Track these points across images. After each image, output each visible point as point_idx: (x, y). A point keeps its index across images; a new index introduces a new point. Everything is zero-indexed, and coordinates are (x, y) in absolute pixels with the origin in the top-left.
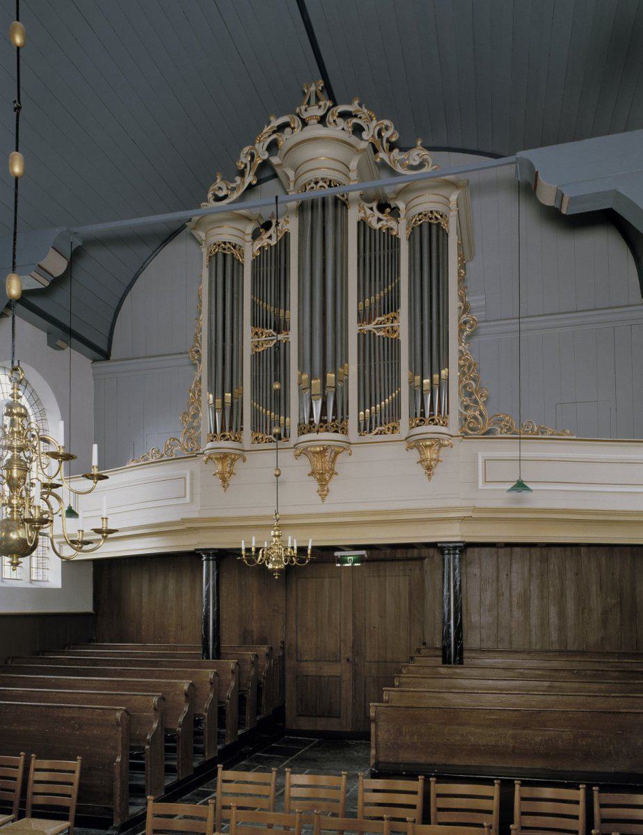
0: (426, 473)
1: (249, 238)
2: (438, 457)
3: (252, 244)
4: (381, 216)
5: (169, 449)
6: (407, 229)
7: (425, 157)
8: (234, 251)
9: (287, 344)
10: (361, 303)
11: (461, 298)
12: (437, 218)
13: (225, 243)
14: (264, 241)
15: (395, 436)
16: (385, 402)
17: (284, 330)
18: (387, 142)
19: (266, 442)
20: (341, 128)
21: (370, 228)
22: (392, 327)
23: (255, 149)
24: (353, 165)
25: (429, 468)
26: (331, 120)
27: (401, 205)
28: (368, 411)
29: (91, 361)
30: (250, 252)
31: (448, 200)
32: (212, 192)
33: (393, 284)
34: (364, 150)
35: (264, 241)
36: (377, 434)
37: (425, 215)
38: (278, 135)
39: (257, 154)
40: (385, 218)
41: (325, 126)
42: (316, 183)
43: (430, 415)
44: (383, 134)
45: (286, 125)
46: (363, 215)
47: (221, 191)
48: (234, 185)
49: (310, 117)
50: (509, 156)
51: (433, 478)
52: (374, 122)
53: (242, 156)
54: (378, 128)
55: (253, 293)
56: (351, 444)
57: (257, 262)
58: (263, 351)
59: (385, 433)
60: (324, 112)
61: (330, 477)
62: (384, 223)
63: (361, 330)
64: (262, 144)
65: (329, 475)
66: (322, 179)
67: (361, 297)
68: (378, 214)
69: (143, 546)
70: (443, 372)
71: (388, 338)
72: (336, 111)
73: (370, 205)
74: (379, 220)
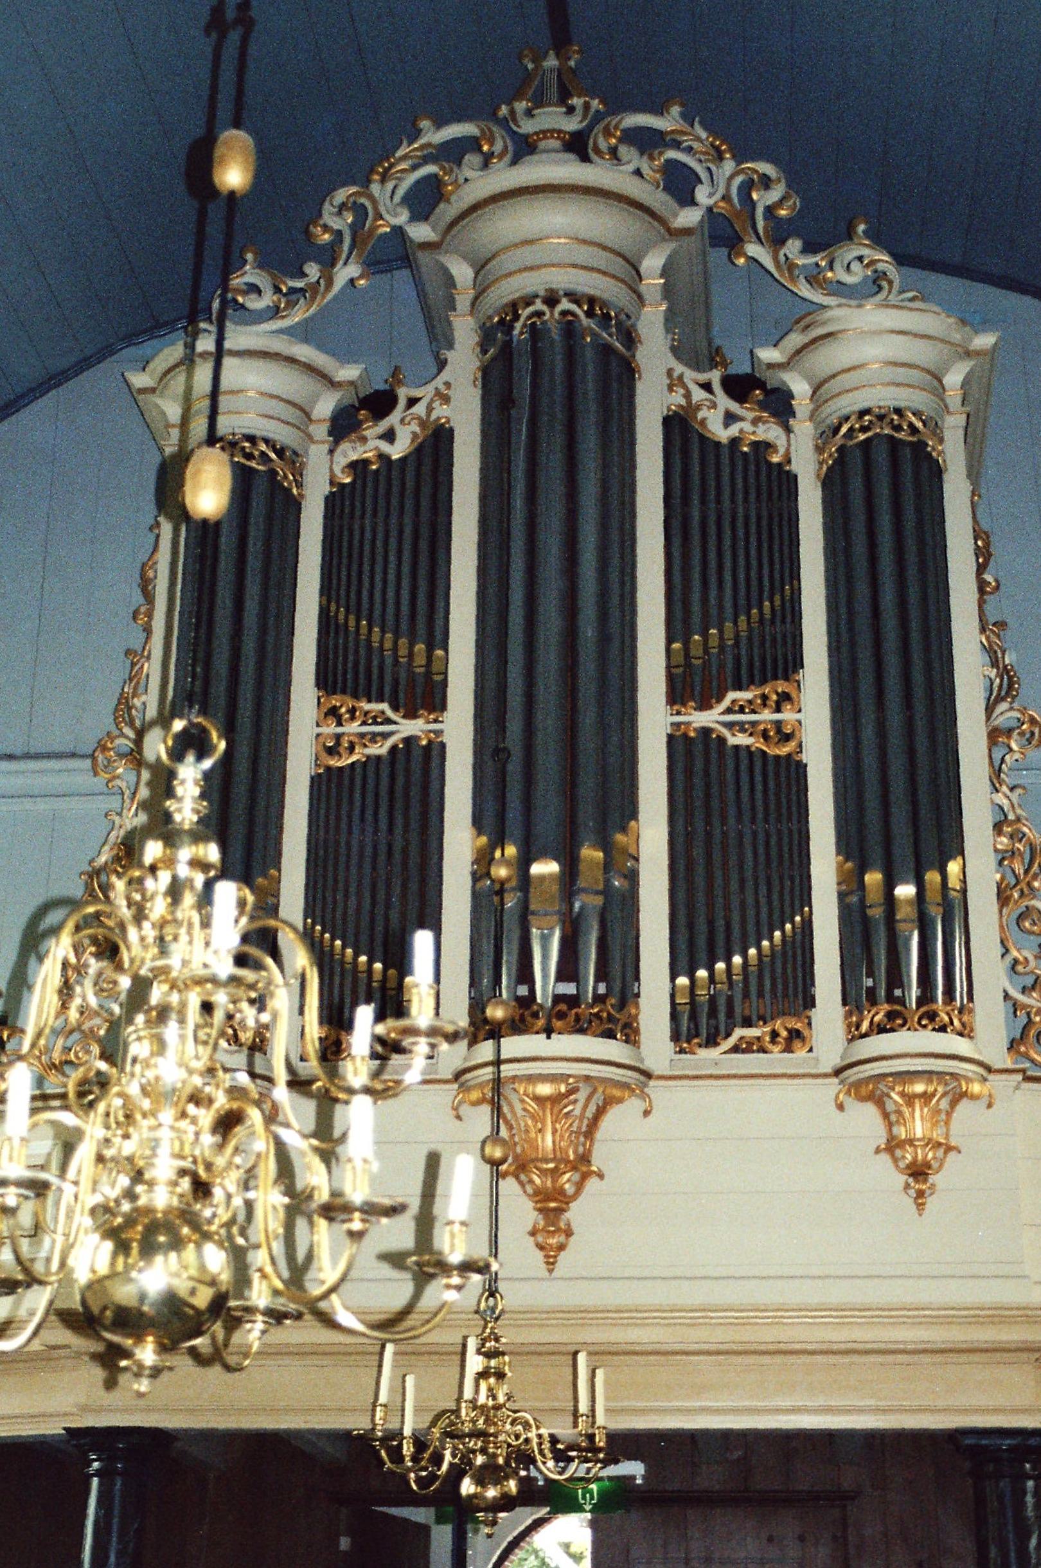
0: (907, 1186)
1: (320, 431)
2: (947, 1136)
3: (331, 452)
4: (734, 407)
6: (819, 449)
7: (881, 266)
11: (993, 656)
12: (913, 430)
13: (252, 439)
18: (765, 218)
20: (631, 168)
21: (703, 438)
22: (778, 724)
23: (371, 197)
24: (653, 263)
25: (919, 1172)
26: (603, 145)
27: (800, 388)
31: (940, 381)
33: (777, 598)
34: (687, 232)
36: (735, 1049)
37: (881, 418)
38: (442, 168)
39: (376, 209)
40: (750, 415)
41: (585, 158)
43: (921, 1002)
44: (755, 196)
45: (471, 144)
46: (683, 402)
47: (253, 296)
48: (299, 284)
49: (544, 132)
50: (156, 354)
51: (931, 1202)
52: (729, 166)
53: (327, 208)
54: (739, 179)
56: (648, 1075)
57: (335, 502)
59: (763, 1050)
61: (579, 1186)
62: (747, 426)
64: (390, 185)
65: (577, 1177)
66: (566, 295)
68: (725, 402)
69: (1001, 1401)
70: (953, 867)
72: (616, 127)
73: (703, 377)
74: (730, 418)
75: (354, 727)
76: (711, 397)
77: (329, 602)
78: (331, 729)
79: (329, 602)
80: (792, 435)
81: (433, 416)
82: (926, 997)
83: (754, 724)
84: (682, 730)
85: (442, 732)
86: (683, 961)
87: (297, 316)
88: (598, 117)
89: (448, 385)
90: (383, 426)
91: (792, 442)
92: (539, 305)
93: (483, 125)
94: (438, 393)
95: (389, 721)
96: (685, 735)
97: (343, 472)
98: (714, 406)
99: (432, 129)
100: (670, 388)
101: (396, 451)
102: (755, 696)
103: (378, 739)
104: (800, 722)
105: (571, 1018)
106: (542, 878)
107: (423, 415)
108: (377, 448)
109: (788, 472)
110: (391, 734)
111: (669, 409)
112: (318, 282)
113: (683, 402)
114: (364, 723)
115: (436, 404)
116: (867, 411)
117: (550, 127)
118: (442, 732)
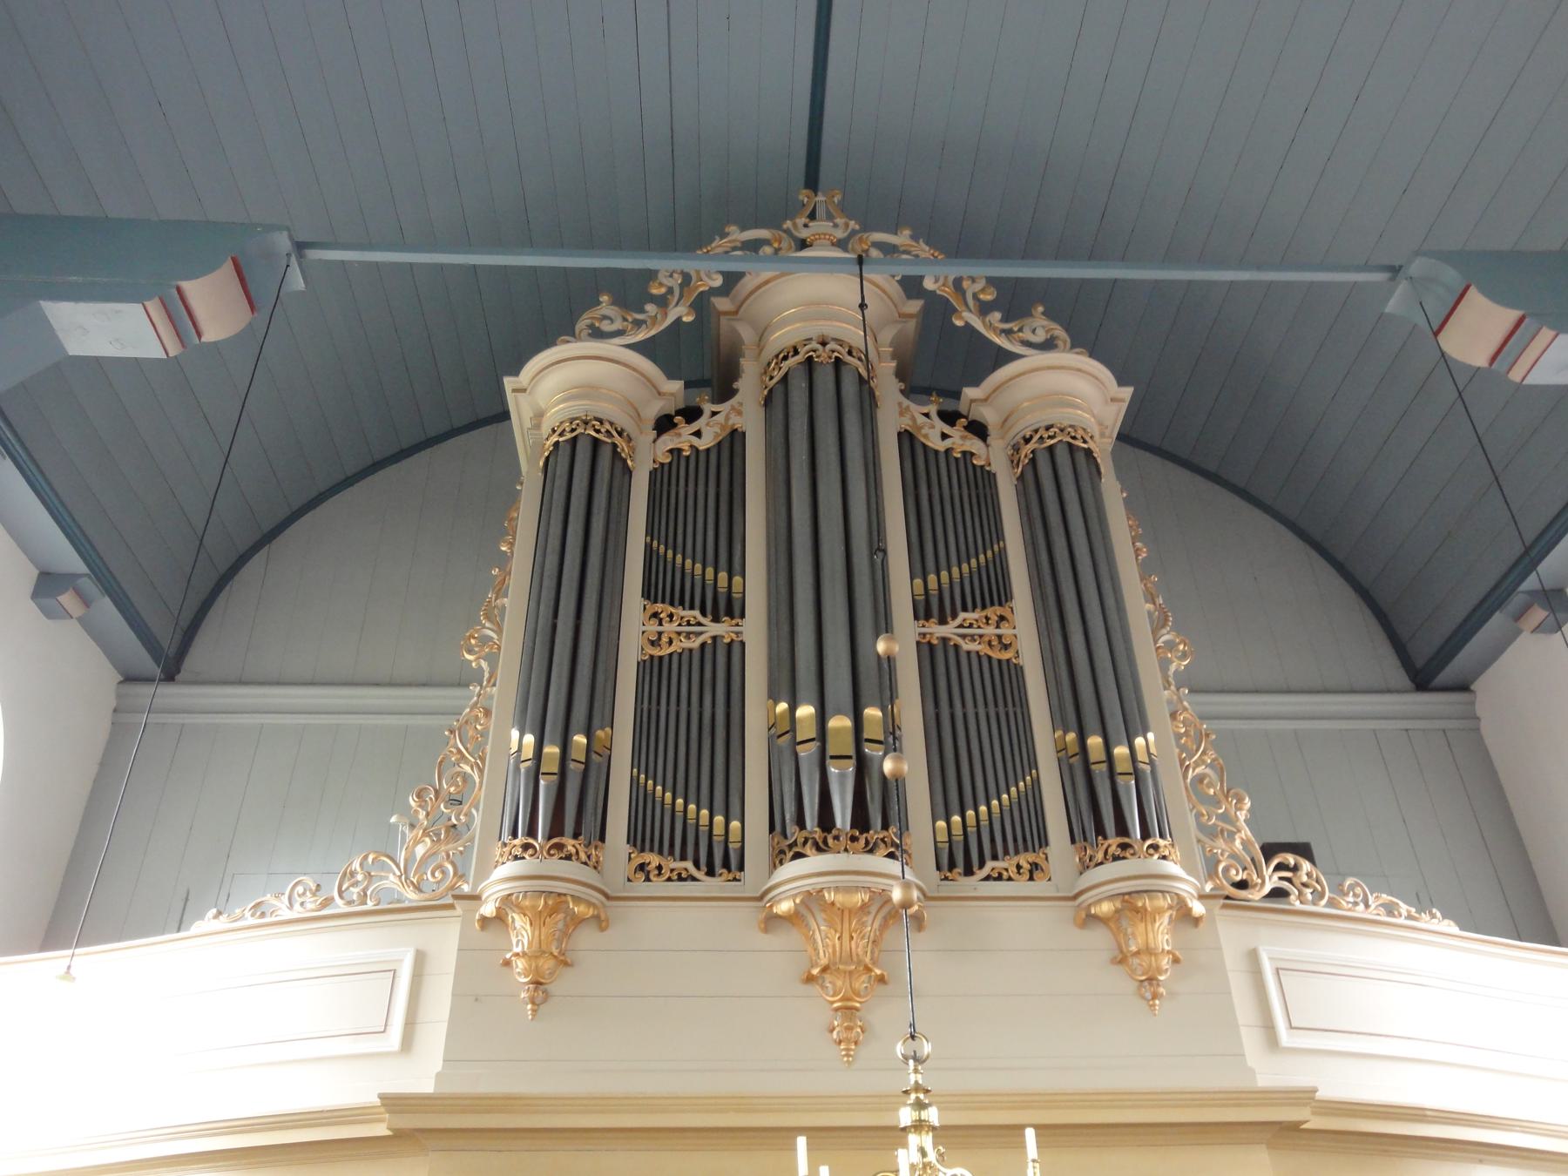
4: (947, 429)
5: (356, 884)
8: (618, 440)
9: (736, 650)
10: (918, 582)
14: (682, 439)
15: (1038, 887)
16: (1009, 793)
17: (726, 615)
19: (669, 879)
21: (925, 446)
22: (1000, 637)
28: (983, 808)
29: (121, 678)
30: (647, 455)
32: (588, 322)
35: (682, 439)
36: (988, 878)
42: (824, 344)
55: (650, 531)
58: (671, 655)
59: (1010, 879)
60: (846, 234)
63: (924, 635)
67: (919, 567)
71: (990, 658)
74: (944, 436)
75: (674, 627)
76: (929, 421)
77: (652, 540)
78: (653, 627)
79: (652, 540)
80: (990, 448)
81: (731, 422)
82: (1146, 834)
83: (981, 636)
84: (927, 640)
85: (741, 633)
86: (941, 809)
87: (641, 336)
88: (854, 233)
89: (741, 404)
90: (695, 427)
91: (991, 453)
92: (814, 345)
93: (774, 231)
94: (733, 408)
95: (699, 624)
96: (929, 643)
97: (663, 454)
98: (933, 427)
99: (738, 231)
100: (901, 414)
101: (703, 444)
102: (980, 617)
103: (691, 636)
104: (1016, 636)
105: (862, 842)
106: (838, 730)
107: (723, 421)
108: (689, 441)
109: (989, 472)
110: (701, 633)
111: (901, 428)
112: (656, 316)
113: (910, 423)
114: (680, 625)
115: (732, 416)
116: (1051, 426)
117: (825, 232)
118: (741, 633)
